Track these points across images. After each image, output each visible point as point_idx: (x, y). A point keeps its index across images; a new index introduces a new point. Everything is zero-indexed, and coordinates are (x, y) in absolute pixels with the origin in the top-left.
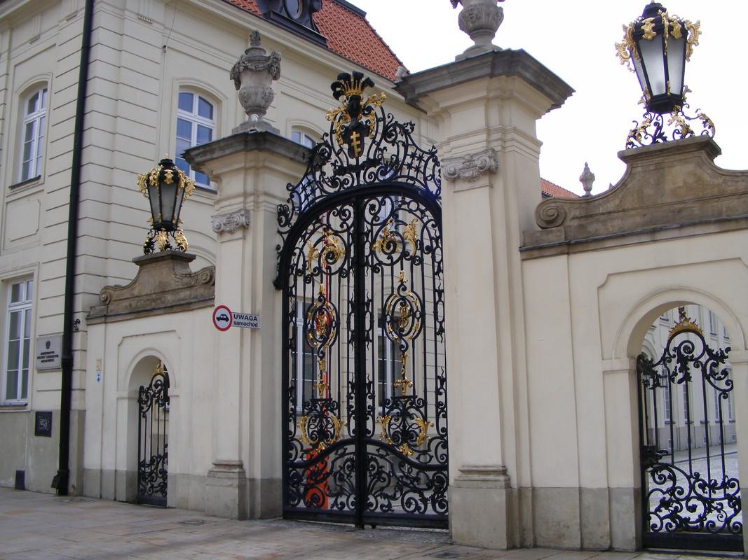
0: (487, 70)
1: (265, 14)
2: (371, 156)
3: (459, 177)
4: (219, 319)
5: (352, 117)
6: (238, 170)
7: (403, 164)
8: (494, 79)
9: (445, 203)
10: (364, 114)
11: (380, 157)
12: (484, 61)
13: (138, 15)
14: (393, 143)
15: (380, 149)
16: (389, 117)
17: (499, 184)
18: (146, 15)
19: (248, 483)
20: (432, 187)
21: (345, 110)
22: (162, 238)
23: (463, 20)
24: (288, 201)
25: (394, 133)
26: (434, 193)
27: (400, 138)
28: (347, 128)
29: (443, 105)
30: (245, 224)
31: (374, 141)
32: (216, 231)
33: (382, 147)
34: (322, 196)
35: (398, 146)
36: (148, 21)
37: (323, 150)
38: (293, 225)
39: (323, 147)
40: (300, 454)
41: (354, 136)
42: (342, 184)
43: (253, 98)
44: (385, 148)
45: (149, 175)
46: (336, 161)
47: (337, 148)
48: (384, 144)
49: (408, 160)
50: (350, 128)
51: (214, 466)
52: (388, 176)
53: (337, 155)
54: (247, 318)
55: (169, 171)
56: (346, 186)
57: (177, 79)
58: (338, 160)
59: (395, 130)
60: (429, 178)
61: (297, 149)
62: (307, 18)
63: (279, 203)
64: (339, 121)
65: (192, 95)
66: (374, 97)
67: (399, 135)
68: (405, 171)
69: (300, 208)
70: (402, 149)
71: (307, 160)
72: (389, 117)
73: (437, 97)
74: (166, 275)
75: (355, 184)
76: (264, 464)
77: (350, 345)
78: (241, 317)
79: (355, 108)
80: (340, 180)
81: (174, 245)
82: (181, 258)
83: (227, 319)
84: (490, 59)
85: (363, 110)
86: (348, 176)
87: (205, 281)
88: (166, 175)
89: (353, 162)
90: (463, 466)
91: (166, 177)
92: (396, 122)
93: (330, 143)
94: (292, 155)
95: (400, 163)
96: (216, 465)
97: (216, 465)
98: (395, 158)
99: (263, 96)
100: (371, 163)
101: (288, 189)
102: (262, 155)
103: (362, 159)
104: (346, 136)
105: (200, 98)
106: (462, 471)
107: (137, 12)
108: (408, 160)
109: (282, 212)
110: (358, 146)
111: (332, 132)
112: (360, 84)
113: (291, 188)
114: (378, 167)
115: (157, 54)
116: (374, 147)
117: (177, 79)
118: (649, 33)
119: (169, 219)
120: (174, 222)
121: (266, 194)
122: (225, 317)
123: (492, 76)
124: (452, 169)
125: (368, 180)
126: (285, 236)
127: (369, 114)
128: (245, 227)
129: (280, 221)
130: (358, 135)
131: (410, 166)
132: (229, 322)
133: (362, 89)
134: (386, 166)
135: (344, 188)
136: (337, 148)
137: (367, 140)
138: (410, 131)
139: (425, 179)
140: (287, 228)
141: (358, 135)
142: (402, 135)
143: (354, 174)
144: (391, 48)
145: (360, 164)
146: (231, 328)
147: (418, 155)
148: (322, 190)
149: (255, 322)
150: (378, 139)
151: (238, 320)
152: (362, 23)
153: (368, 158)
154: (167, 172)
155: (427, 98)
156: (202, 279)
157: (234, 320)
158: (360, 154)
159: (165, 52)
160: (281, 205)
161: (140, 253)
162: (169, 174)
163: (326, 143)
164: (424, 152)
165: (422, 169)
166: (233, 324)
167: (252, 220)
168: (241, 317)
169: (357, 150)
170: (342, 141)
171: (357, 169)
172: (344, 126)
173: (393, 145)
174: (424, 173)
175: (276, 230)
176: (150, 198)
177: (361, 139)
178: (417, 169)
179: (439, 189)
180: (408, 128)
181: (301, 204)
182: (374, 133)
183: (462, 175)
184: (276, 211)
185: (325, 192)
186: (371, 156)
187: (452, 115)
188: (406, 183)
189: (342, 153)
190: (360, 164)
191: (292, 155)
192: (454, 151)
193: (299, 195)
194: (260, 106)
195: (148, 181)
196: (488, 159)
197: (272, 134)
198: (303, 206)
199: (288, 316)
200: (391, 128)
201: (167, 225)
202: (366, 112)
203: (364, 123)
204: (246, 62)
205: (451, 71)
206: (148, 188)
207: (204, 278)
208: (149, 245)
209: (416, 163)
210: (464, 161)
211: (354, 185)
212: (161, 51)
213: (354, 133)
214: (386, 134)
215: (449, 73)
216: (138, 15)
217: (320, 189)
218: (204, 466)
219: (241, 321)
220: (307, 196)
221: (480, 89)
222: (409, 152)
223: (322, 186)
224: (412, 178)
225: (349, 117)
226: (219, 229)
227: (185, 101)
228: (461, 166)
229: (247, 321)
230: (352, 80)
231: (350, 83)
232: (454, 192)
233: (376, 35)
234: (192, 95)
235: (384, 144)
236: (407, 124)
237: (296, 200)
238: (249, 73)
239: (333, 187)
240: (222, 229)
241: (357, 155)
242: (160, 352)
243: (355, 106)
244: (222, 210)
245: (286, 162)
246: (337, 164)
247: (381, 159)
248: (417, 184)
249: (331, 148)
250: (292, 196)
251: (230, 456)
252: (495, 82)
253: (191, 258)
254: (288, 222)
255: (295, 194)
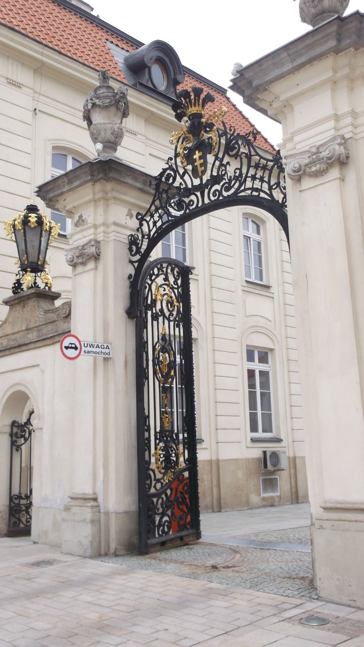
0: (332, 43)
1: (133, 85)
2: (215, 174)
3: (305, 173)
4: (67, 348)
5: (194, 136)
6: (89, 202)
7: (247, 176)
8: (340, 54)
9: (291, 211)
10: (206, 132)
11: (223, 173)
12: (329, 31)
13: (7, 79)
14: (236, 156)
15: (223, 165)
16: (230, 130)
17: (351, 175)
18: (15, 79)
19: (102, 516)
20: (278, 195)
21: (187, 131)
22: (28, 279)
23: (304, 6)
24: (138, 230)
25: (236, 146)
26: (280, 202)
27: (244, 150)
28: (190, 149)
29: (283, 97)
30: (95, 254)
31: (217, 158)
32: (70, 264)
33: (224, 162)
34: (169, 221)
35: (241, 159)
36: (18, 85)
37: (168, 174)
38: (143, 252)
39: (168, 172)
40: (153, 483)
41: (197, 155)
42: (187, 208)
43: (102, 134)
44: (228, 163)
45: (15, 220)
46: (181, 184)
47: (181, 171)
48: (226, 159)
49: (252, 172)
50: (193, 148)
51: (70, 500)
52: (232, 191)
53: (182, 177)
54: (98, 346)
55: (33, 215)
56: (191, 208)
57: (49, 140)
58: (183, 183)
59: (237, 143)
60: (274, 187)
61: (145, 178)
62: (172, 90)
63: (129, 233)
64: (182, 143)
65: (66, 155)
66: (215, 112)
67: (242, 147)
68: (249, 184)
69: (149, 235)
70: (245, 161)
71: (154, 187)
72: (230, 130)
73: (278, 88)
74: (35, 312)
75: (200, 204)
76: (118, 498)
77: (146, 340)
78: (92, 346)
79: (197, 126)
80: (185, 202)
81: (42, 286)
82: (48, 296)
83: (76, 348)
84: (334, 28)
85: (205, 128)
86: (193, 197)
87: (65, 316)
88: (30, 219)
89: (197, 182)
90: (326, 502)
91: (29, 221)
92: (238, 134)
93: (174, 167)
94: (139, 185)
95: (244, 176)
96: (72, 498)
97: (72, 498)
98: (238, 171)
99: (112, 131)
100: (215, 180)
101: (137, 218)
102: (109, 186)
103: (206, 178)
104: (189, 158)
105: (73, 158)
106: (324, 508)
107: (5, 76)
108: (252, 172)
109: (133, 242)
110: (201, 165)
111: (177, 155)
112: (201, 101)
113: (140, 217)
114: (222, 184)
115: (28, 116)
116: (217, 163)
117: (49, 140)
118: (33, 223)
119: (36, 261)
120: (39, 263)
121: (115, 224)
122: (73, 346)
123: (337, 51)
124: (297, 166)
125: (213, 198)
126: (136, 265)
127: (211, 130)
128: (97, 257)
129: (130, 250)
130: (201, 154)
131: (254, 178)
132: (78, 350)
133: (203, 106)
134: (230, 180)
135: (189, 209)
136: (181, 171)
137: (210, 158)
138: (253, 139)
139: (270, 188)
140: (138, 257)
141: (201, 154)
142: (245, 146)
143: (198, 194)
144: (250, 120)
145: (204, 182)
146: (80, 356)
147: (261, 165)
148: (169, 214)
149: (107, 351)
150: (220, 156)
151: (89, 349)
152: (224, 99)
153: (212, 176)
154: (30, 217)
155: (266, 92)
156: (62, 313)
157: (83, 349)
158: (203, 172)
159: (36, 114)
160: (131, 235)
161: (9, 294)
162: (33, 218)
163: (171, 168)
164: (268, 160)
165: (266, 179)
166: (82, 352)
167: (102, 251)
168: (92, 346)
169: (200, 169)
170: (185, 163)
171: (201, 188)
172: (187, 147)
173: (236, 158)
174: (269, 183)
175: (127, 260)
176: (16, 242)
177: (203, 157)
178: (262, 180)
179: (285, 197)
180: (251, 138)
181: (150, 231)
182: (216, 150)
183: (308, 170)
184: (127, 242)
185: (172, 216)
186: (215, 174)
187: (295, 108)
188: (251, 195)
189: (187, 175)
190: (204, 182)
191: (139, 185)
192: (298, 146)
193: (148, 223)
194: (110, 142)
195: (14, 226)
196: (337, 147)
197: (115, 161)
198: (152, 233)
199: (141, 346)
200: (234, 141)
201: (36, 267)
202: (208, 129)
203: (207, 141)
204: (94, 99)
205: (291, 52)
206: (14, 232)
207: (64, 312)
208: (18, 286)
209: (259, 174)
210: (309, 155)
211: (199, 205)
212: (31, 114)
213: (197, 152)
214: (229, 148)
215: (289, 55)
216: (7, 79)
217: (167, 214)
218: (60, 498)
219: (92, 349)
220: (155, 223)
221: (322, 71)
222: (253, 164)
223: (168, 210)
224: (257, 190)
225: (192, 138)
226: (72, 261)
227: (250, 358)
228: (307, 161)
229: (98, 350)
230: (192, 97)
231: (190, 101)
232: (300, 191)
233: (237, 109)
234: (66, 155)
235: (226, 159)
236: (249, 133)
237: (145, 229)
238: (98, 110)
239: (179, 210)
240: (75, 261)
241: (200, 174)
242: (26, 386)
243: (196, 123)
244: (75, 243)
245: (135, 193)
246: (182, 187)
247: (224, 175)
248: (262, 195)
249: (176, 171)
250: (141, 225)
251: (85, 488)
252: (343, 59)
253: (56, 296)
254: (138, 251)
255: (144, 223)
